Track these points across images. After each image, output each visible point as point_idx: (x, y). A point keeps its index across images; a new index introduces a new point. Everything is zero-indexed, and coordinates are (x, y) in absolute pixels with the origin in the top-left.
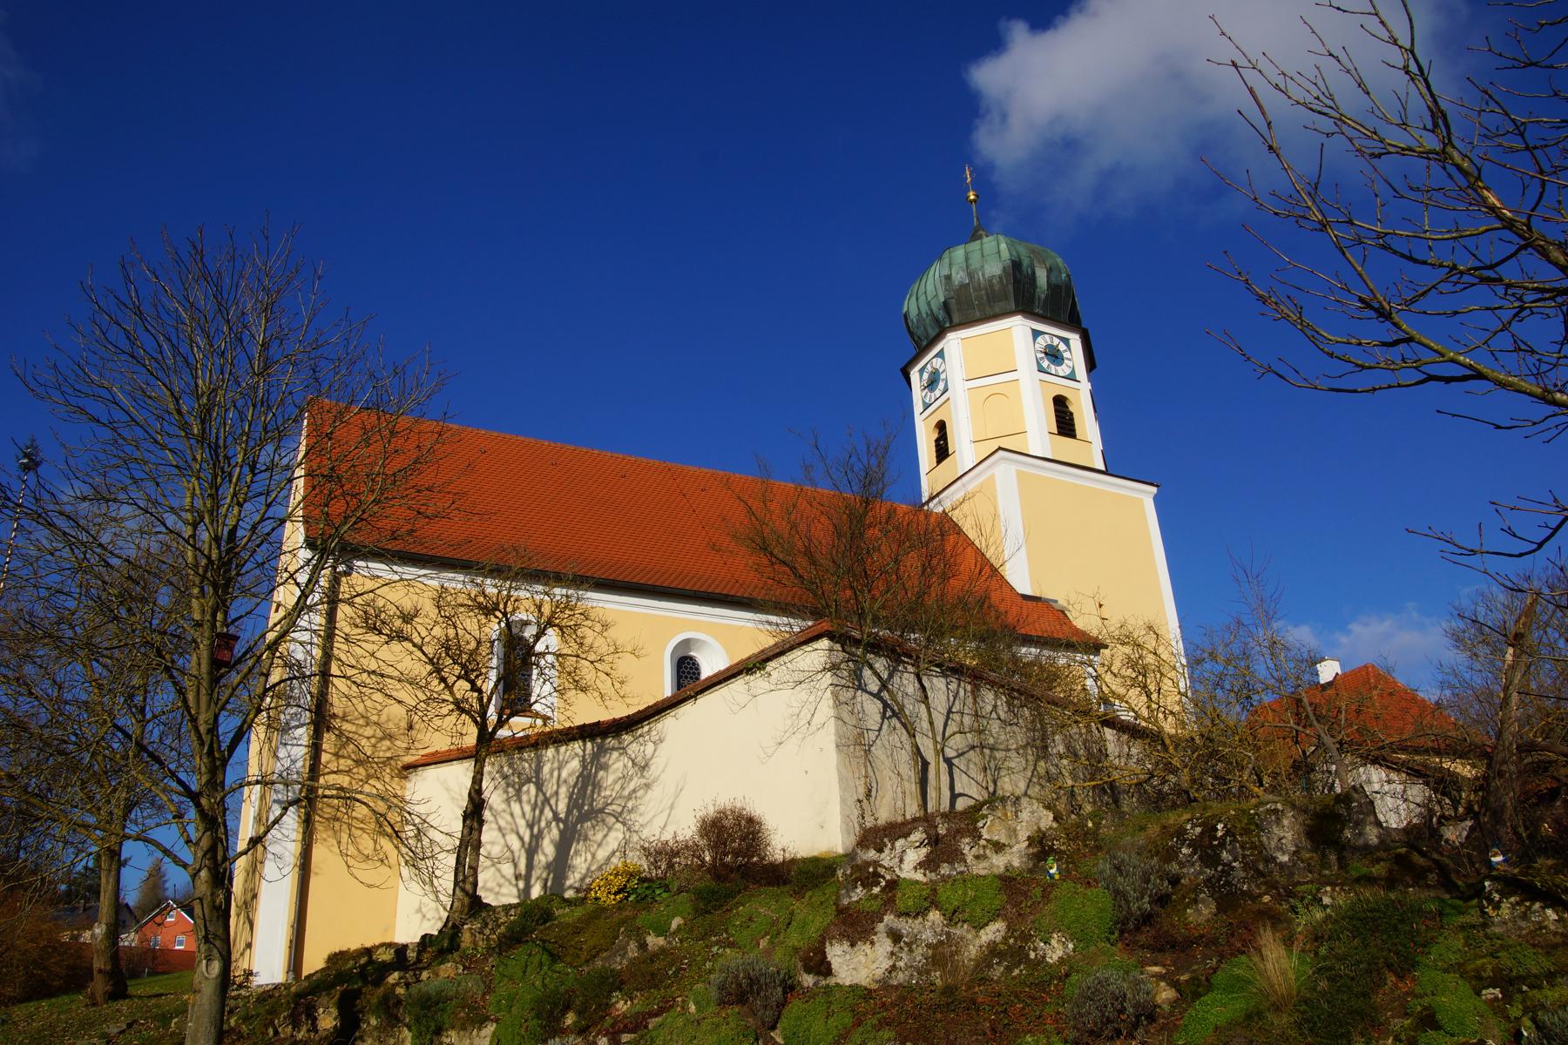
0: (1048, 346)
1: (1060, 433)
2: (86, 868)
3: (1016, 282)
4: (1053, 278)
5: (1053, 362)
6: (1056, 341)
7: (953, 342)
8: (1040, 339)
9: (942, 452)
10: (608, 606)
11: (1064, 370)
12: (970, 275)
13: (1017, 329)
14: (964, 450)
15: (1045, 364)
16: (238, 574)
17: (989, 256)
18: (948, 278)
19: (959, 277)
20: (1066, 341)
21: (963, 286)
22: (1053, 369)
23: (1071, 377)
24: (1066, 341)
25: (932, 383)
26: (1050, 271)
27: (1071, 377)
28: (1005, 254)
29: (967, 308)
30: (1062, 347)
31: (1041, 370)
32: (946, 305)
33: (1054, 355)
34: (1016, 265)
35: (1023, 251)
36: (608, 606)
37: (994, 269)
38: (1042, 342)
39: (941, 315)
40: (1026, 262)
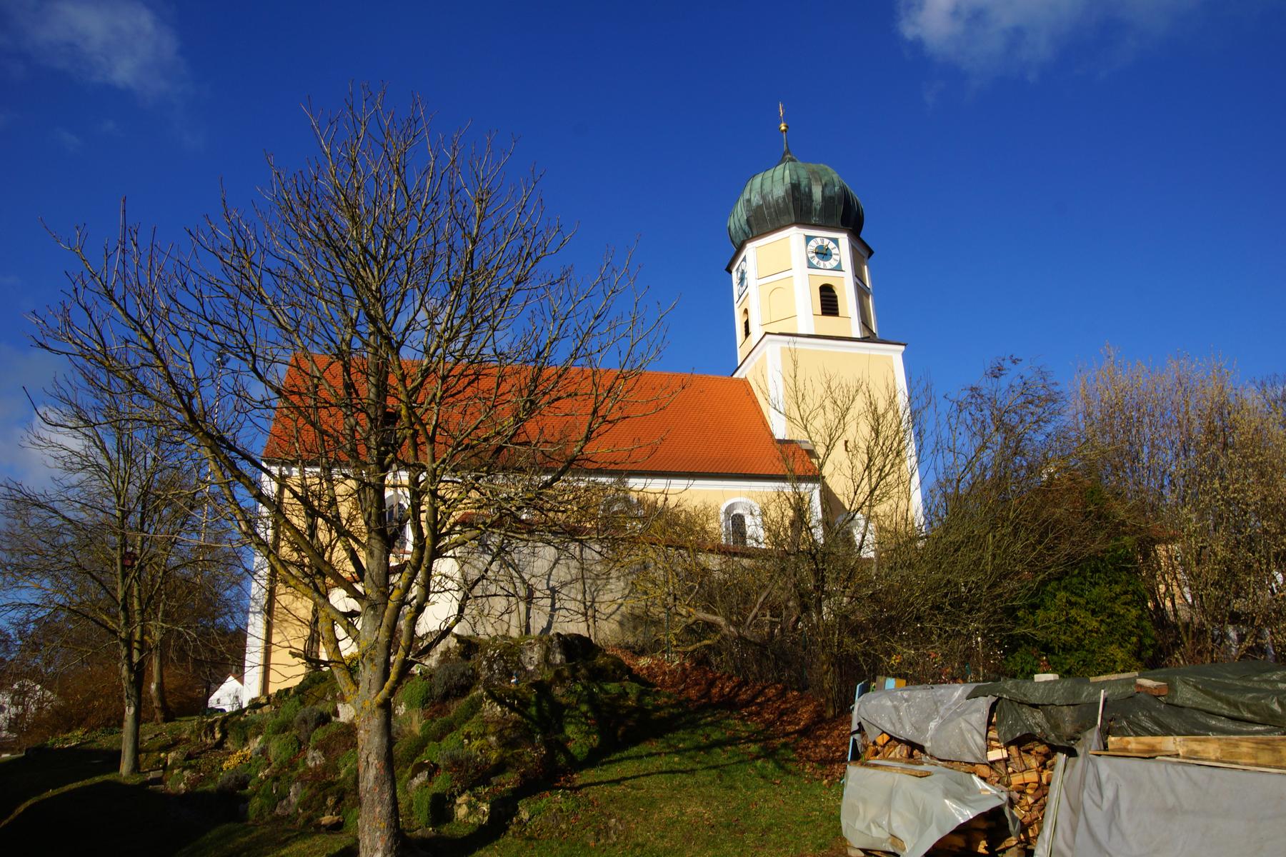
0: (820, 247)
1: (824, 314)
2: (154, 459)
3: (795, 199)
4: (827, 192)
5: (822, 259)
6: (826, 242)
7: (751, 249)
8: (812, 243)
9: (747, 333)
10: (873, 353)
11: (832, 263)
12: (763, 197)
13: (794, 235)
14: (756, 332)
15: (815, 261)
16: (389, 329)
17: (773, 183)
18: (749, 201)
19: (756, 200)
20: (835, 241)
21: (760, 207)
22: (822, 264)
23: (839, 268)
24: (835, 241)
25: (742, 279)
26: (824, 186)
27: (839, 268)
28: (787, 180)
29: (764, 222)
30: (832, 245)
31: (811, 266)
32: (748, 220)
33: (824, 253)
34: (795, 187)
35: (803, 174)
36: (873, 353)
37: (779, 191)
38: (813, 244)
39: (747, 229)
40: (804, 183)
